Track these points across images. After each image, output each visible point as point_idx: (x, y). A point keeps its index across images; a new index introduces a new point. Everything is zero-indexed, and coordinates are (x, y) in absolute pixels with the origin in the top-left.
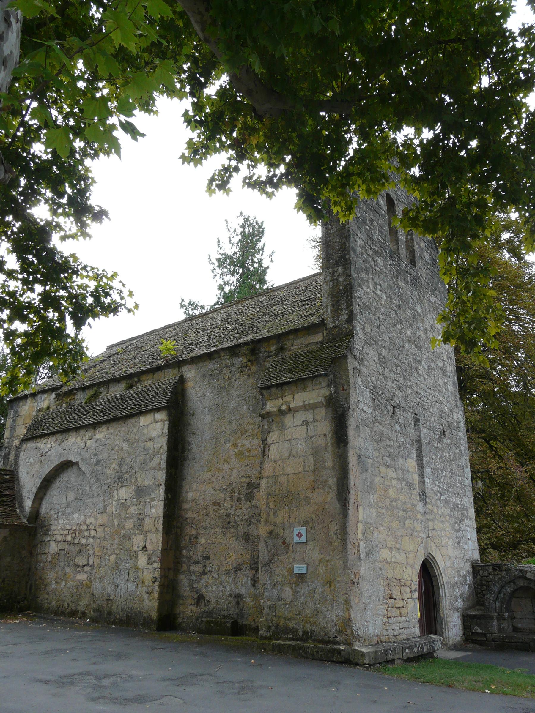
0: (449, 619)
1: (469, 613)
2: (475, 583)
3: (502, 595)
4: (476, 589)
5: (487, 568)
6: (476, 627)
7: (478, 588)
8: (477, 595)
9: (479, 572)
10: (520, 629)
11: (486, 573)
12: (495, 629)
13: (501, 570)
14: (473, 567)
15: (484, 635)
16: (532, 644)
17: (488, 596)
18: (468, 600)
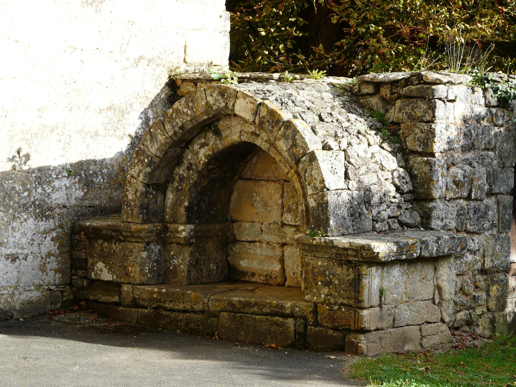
6: (100, 265)
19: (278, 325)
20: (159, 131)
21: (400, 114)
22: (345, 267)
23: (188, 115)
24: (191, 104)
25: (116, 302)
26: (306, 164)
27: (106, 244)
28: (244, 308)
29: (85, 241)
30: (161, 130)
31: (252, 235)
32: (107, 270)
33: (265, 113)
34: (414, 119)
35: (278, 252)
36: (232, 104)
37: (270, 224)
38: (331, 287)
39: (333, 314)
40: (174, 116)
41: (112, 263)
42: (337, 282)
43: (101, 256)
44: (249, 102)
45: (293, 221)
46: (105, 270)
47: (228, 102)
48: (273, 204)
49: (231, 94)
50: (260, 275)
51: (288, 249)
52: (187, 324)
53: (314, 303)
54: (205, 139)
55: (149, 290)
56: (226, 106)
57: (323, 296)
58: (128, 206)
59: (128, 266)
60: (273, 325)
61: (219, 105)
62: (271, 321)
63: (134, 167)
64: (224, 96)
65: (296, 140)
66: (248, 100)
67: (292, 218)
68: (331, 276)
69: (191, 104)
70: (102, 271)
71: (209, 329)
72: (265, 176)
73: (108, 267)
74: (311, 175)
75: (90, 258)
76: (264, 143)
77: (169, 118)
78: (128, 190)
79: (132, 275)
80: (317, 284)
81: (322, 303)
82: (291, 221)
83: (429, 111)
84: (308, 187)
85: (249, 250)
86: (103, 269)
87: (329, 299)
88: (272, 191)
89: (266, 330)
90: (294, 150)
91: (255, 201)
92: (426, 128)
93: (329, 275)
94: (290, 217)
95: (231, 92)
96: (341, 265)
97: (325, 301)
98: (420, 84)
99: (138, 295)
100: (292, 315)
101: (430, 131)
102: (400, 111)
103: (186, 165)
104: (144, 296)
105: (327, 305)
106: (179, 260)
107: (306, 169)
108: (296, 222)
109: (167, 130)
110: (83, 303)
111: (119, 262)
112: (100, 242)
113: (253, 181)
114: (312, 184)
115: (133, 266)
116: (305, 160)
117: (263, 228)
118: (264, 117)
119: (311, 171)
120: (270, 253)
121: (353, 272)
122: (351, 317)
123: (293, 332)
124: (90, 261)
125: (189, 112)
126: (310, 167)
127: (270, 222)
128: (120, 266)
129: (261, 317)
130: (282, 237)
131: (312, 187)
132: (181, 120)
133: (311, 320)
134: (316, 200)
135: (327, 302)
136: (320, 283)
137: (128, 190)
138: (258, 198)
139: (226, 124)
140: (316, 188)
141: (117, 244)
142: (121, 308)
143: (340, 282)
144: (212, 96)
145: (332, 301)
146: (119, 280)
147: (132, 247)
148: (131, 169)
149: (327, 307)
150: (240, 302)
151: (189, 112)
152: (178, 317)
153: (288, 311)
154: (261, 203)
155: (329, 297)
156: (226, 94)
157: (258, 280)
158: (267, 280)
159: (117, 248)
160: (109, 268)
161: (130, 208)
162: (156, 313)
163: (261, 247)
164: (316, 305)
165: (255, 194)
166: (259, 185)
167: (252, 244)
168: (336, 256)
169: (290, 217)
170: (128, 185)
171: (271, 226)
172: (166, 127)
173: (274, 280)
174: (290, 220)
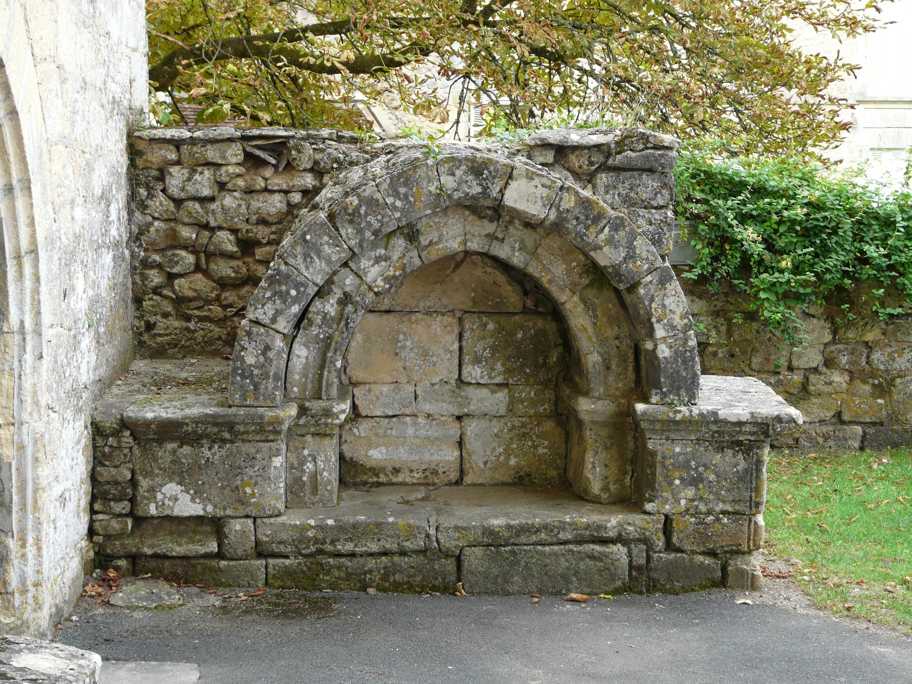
0: (45, 471)
1: (132, 412)
2: (136, 237)
3: (330, 307)
4: (140, 267)
5: (212, 153)
6: (172, 488)
7: (146, 264)
8: (138, 301)
9: (162, 176)
10: (375, 471)
11: (203, 183)
12: (274, 494)
13: (290, 167)
14: (134, 150)
15: (215, 525)
16: (474, 558)
17: (264, 313)
18: (111, 333)
19: (592, 557)
20: (326, 238)
21: (608, 196)
22: (730, 452)
23: (394, 208)
24: (402, 190)
25: (212, 552)
26: (652, 288)
27: (186, 449)
28: (518, 535)
29: (131, 448)
30: (330, 237)
31: (396, 405)
32: (188, 497)
33: (572, 204)
34: (636, 204)
35: (454, 430)
36: (498, 189)
37: (433, 385)
38: (701, 486)
39: (705, 529)
40: (362, 212)
41: (203, 483)
42: (712, 477)
43: (174, 473)
44: (539, 186)
45: (486, 377)
46: (185, 498)
47: (490, 185)
48: (441, 351)
49: (497, 171)
50: (412, 471)
51: (474, 424)
52: (385, 577)
53: (666, 516)
54: (386, 249)
55: (296, 525)
56: (485, 192)
57: (683, 502)
58: (243, 377)
59: (244, 486)
60: (582, 559)
61: (468, 191)
62: (579, 552)
63: (263, 305)
64: (482, 174)
65: (635, 248)
66: (537, 181)
67: (482, 372)
68: (701, 469)
69: (402, 190)
70: (176, 499)
71: (436, 579)
72: (422, 305)
73: (192, 492)
74: (664, 306)
75: (145, 478)
76: (517, 254)
77: (349, 215)
78: (243, 348)
79: (253, 500)
80: (671, 483)
81: (681, 513)
82: (482, 378)
83: (664, 191)
84: (656, 326)
85: (389, 431)
86: (179, 496)
87: (697, 507)
88: (438, 329)
89: (568, 569)
90: (631, 266)
91: (404, 347)
92: (657, 217)
93: (697, 468)
94: (479, 371)
95: (499, 167)
96: (721, 449)
97: (688, 510)
98: (647, 148)
99: (268, 536)
100: (619, 539)
101: (666, 222)
102: (607, 192)
103: (337, 296)
104: (284, 536)
105: (692, 515)
106: (319, 463)
107: (653, 296)
108: (491, 378)
109: (344, 236)
110: (122, 563)
111: (220, 479)
112: (170, 446)
113: (396, 314)
114: (665, 321)
115: (256, 484)
116: (651, 282)
117: (419, 392)
118: (568, 211)
119: (663, 300)
120: (434, 432)
121: (744, 459)
122: (741, 531)
123: (626, 568)
124: (144, 483)
125: (399, 204)
126: (661, 293)
127: (434, 382)
128: (223, 488)
129: (556, 548)
130: (460, 405)
131: (665, 325)
132: (379, 217)
133: (660, 543)
134: (671, 347)
135: (692, 511)
136: (677, 482)
137: (243, 348)
138: (408, 343)
139: (435, 223)
140: (673, 327)
141: (216, 447)
142: (223, 562)
143: (718, 476)
144: (453, 174)
145: (703, 508)
146: (220, 513)
147: (253, 451)
148: (256, 309)
149: (693, 520)
150: (509, 527)
151: (399, 204)
152: (363, 566)
153: (612, 534)
154: (416, 350)
155: (696, 503)
156: (486, 172)
157: (407, 480)
158: (426, 477)
159: (214, 454)
160: (196, 493)
161: (252, 380)
162: (312, 563)
163: (415, 424)
164: (668, 520)
165: (401, 337)
166: (410, 320)
167: (394, 419)
168: (713, 436)
169: (479, 371)
170: (246, 338)
171: (437, 387)
172: (343, 232)
173: (442, 476)
174: (479, 375)
